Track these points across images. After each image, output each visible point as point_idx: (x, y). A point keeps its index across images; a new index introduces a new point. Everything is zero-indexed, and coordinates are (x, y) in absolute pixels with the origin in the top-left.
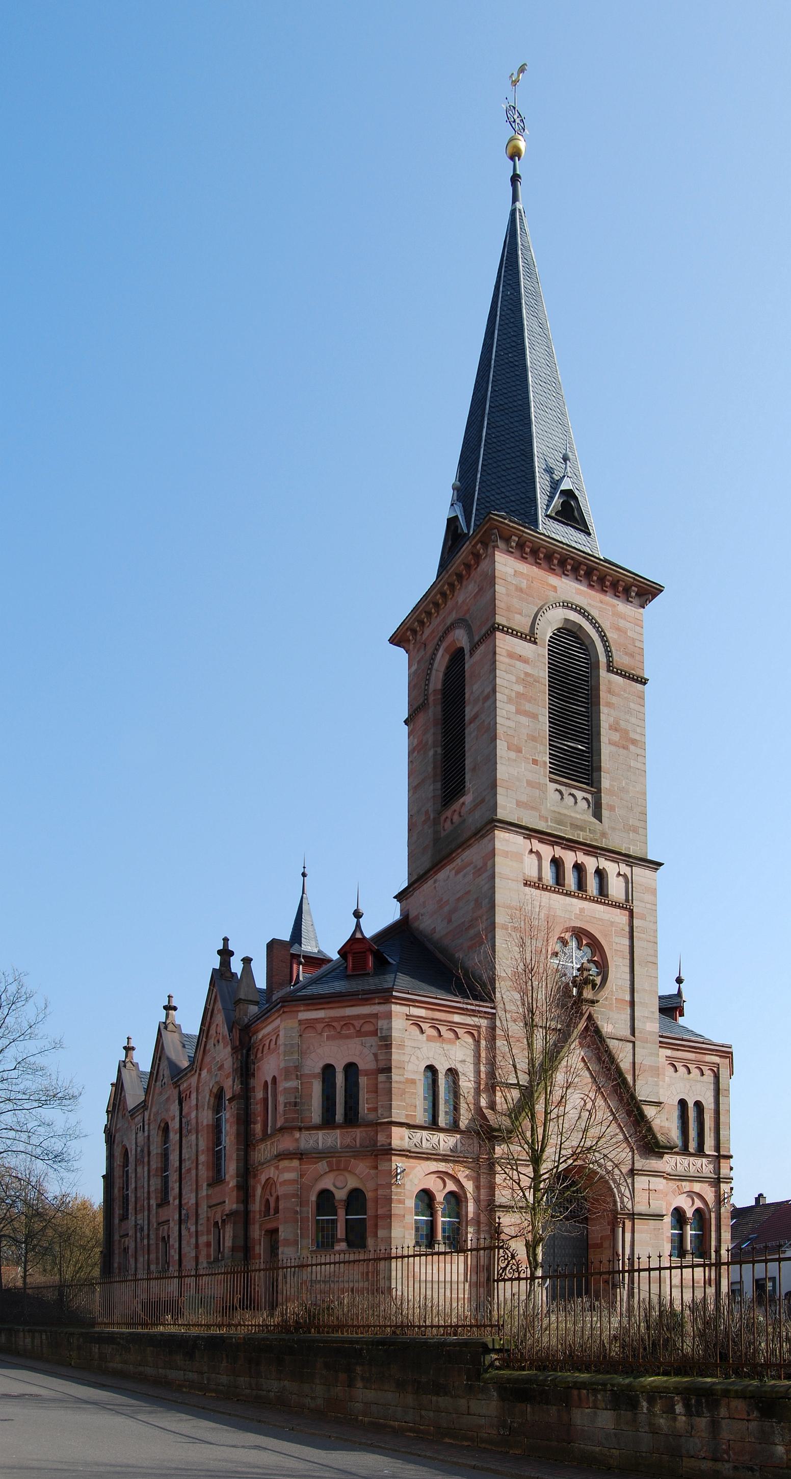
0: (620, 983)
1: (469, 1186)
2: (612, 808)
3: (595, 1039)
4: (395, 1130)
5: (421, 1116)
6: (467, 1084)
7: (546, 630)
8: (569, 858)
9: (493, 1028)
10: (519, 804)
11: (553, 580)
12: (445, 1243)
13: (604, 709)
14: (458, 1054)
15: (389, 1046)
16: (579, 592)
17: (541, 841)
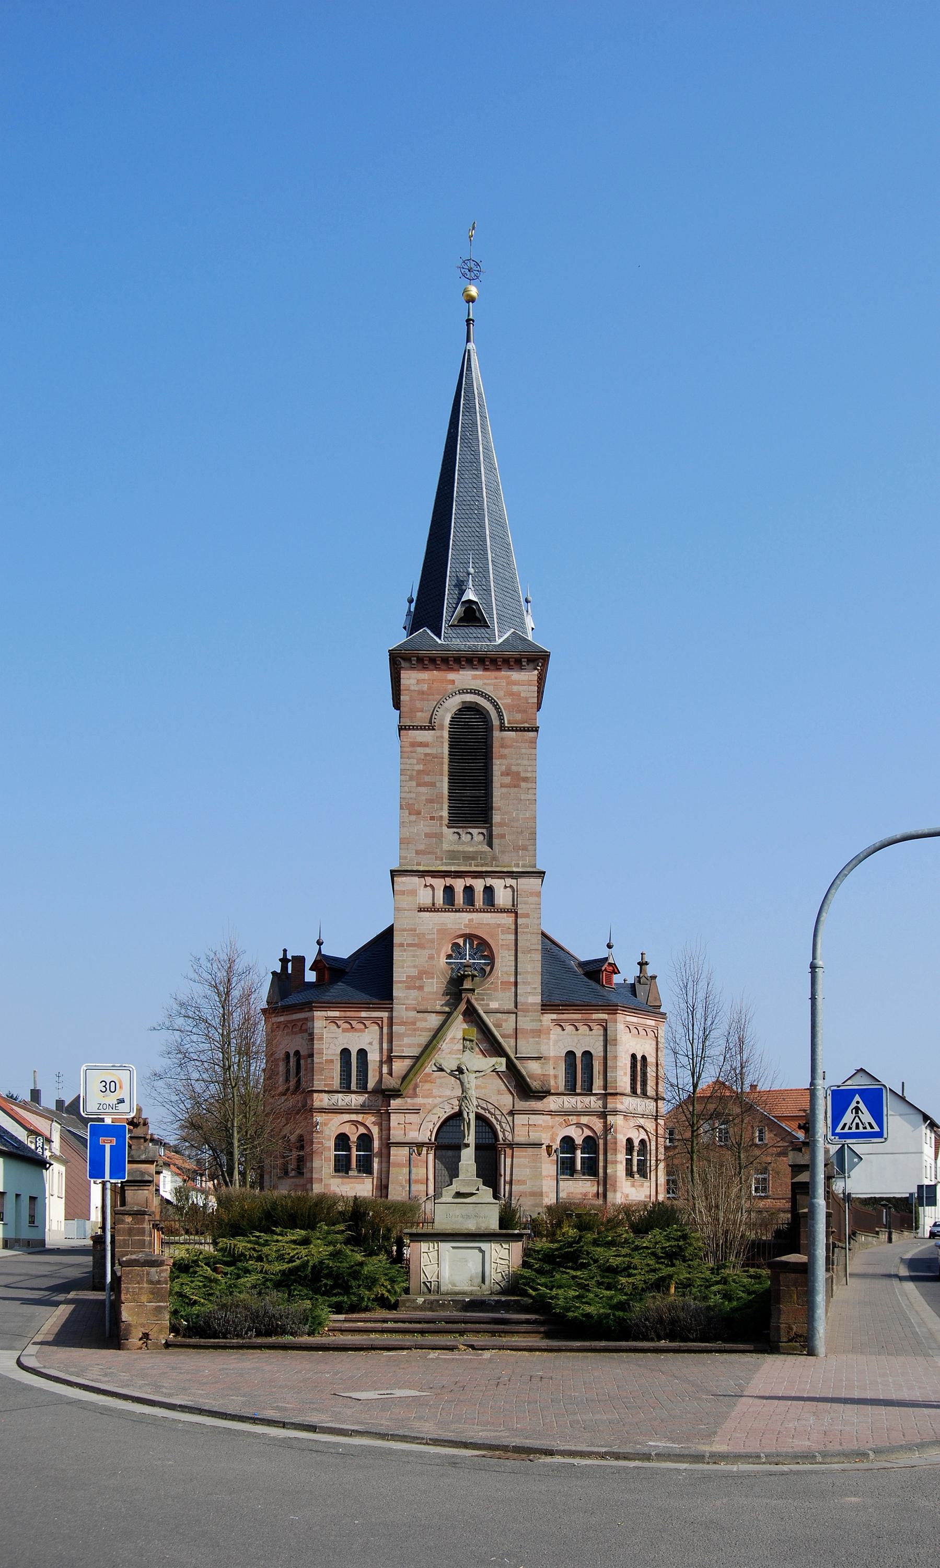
0: (505, 969)
1: (375, 1131)
2: (503, 836)
3: (471, 1015)
4: (315, 1095)
5: (336, 1083)
6: (373, 1057)
7: (446, 718)
8: (459, 885)
9: (391, 1019)
10: (418, 852)
11: (451, 676)
12: (642, 1238)
13: (496, 762)
14: (366, 1039)
15: (312, 1040)
16: (475, 678)
17: (433, 877)
